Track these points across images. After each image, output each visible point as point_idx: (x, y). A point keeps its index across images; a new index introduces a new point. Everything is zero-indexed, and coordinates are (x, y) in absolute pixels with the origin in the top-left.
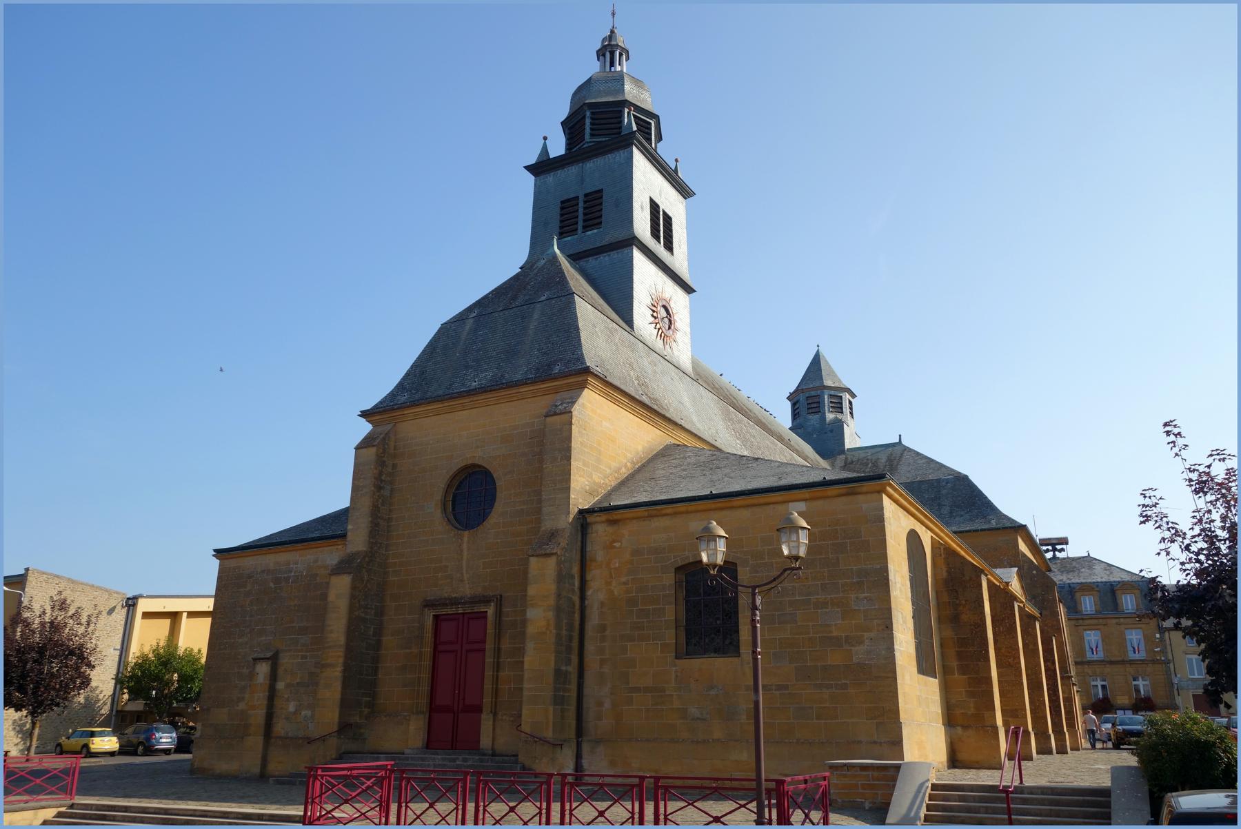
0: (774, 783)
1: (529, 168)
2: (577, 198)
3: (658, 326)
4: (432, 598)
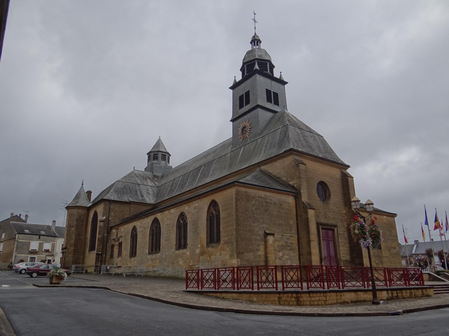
2: (243, 95)
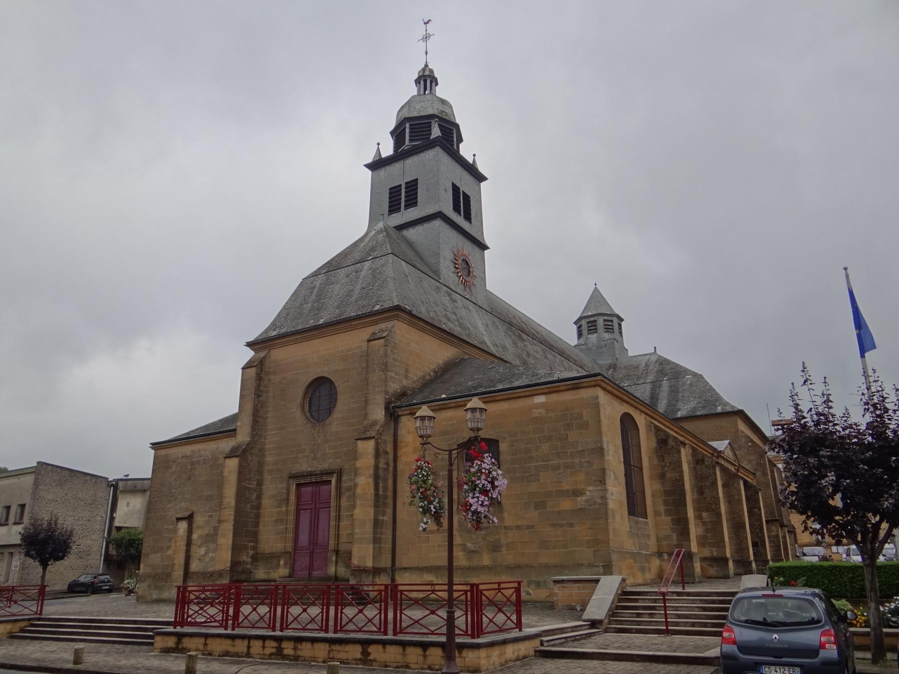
0: (469, 586)
1: (368, 166)
2: (400, 186)
3: (459, 274)
4: (295, 472)
